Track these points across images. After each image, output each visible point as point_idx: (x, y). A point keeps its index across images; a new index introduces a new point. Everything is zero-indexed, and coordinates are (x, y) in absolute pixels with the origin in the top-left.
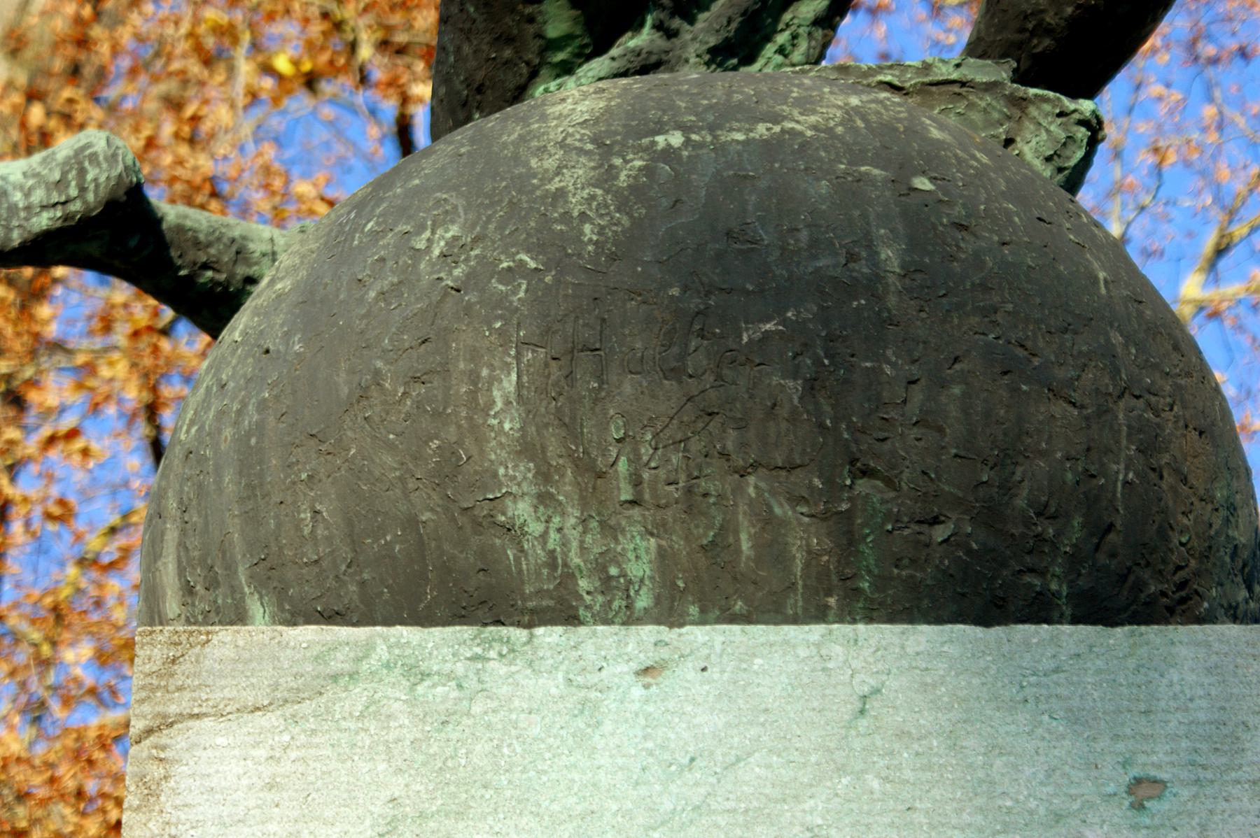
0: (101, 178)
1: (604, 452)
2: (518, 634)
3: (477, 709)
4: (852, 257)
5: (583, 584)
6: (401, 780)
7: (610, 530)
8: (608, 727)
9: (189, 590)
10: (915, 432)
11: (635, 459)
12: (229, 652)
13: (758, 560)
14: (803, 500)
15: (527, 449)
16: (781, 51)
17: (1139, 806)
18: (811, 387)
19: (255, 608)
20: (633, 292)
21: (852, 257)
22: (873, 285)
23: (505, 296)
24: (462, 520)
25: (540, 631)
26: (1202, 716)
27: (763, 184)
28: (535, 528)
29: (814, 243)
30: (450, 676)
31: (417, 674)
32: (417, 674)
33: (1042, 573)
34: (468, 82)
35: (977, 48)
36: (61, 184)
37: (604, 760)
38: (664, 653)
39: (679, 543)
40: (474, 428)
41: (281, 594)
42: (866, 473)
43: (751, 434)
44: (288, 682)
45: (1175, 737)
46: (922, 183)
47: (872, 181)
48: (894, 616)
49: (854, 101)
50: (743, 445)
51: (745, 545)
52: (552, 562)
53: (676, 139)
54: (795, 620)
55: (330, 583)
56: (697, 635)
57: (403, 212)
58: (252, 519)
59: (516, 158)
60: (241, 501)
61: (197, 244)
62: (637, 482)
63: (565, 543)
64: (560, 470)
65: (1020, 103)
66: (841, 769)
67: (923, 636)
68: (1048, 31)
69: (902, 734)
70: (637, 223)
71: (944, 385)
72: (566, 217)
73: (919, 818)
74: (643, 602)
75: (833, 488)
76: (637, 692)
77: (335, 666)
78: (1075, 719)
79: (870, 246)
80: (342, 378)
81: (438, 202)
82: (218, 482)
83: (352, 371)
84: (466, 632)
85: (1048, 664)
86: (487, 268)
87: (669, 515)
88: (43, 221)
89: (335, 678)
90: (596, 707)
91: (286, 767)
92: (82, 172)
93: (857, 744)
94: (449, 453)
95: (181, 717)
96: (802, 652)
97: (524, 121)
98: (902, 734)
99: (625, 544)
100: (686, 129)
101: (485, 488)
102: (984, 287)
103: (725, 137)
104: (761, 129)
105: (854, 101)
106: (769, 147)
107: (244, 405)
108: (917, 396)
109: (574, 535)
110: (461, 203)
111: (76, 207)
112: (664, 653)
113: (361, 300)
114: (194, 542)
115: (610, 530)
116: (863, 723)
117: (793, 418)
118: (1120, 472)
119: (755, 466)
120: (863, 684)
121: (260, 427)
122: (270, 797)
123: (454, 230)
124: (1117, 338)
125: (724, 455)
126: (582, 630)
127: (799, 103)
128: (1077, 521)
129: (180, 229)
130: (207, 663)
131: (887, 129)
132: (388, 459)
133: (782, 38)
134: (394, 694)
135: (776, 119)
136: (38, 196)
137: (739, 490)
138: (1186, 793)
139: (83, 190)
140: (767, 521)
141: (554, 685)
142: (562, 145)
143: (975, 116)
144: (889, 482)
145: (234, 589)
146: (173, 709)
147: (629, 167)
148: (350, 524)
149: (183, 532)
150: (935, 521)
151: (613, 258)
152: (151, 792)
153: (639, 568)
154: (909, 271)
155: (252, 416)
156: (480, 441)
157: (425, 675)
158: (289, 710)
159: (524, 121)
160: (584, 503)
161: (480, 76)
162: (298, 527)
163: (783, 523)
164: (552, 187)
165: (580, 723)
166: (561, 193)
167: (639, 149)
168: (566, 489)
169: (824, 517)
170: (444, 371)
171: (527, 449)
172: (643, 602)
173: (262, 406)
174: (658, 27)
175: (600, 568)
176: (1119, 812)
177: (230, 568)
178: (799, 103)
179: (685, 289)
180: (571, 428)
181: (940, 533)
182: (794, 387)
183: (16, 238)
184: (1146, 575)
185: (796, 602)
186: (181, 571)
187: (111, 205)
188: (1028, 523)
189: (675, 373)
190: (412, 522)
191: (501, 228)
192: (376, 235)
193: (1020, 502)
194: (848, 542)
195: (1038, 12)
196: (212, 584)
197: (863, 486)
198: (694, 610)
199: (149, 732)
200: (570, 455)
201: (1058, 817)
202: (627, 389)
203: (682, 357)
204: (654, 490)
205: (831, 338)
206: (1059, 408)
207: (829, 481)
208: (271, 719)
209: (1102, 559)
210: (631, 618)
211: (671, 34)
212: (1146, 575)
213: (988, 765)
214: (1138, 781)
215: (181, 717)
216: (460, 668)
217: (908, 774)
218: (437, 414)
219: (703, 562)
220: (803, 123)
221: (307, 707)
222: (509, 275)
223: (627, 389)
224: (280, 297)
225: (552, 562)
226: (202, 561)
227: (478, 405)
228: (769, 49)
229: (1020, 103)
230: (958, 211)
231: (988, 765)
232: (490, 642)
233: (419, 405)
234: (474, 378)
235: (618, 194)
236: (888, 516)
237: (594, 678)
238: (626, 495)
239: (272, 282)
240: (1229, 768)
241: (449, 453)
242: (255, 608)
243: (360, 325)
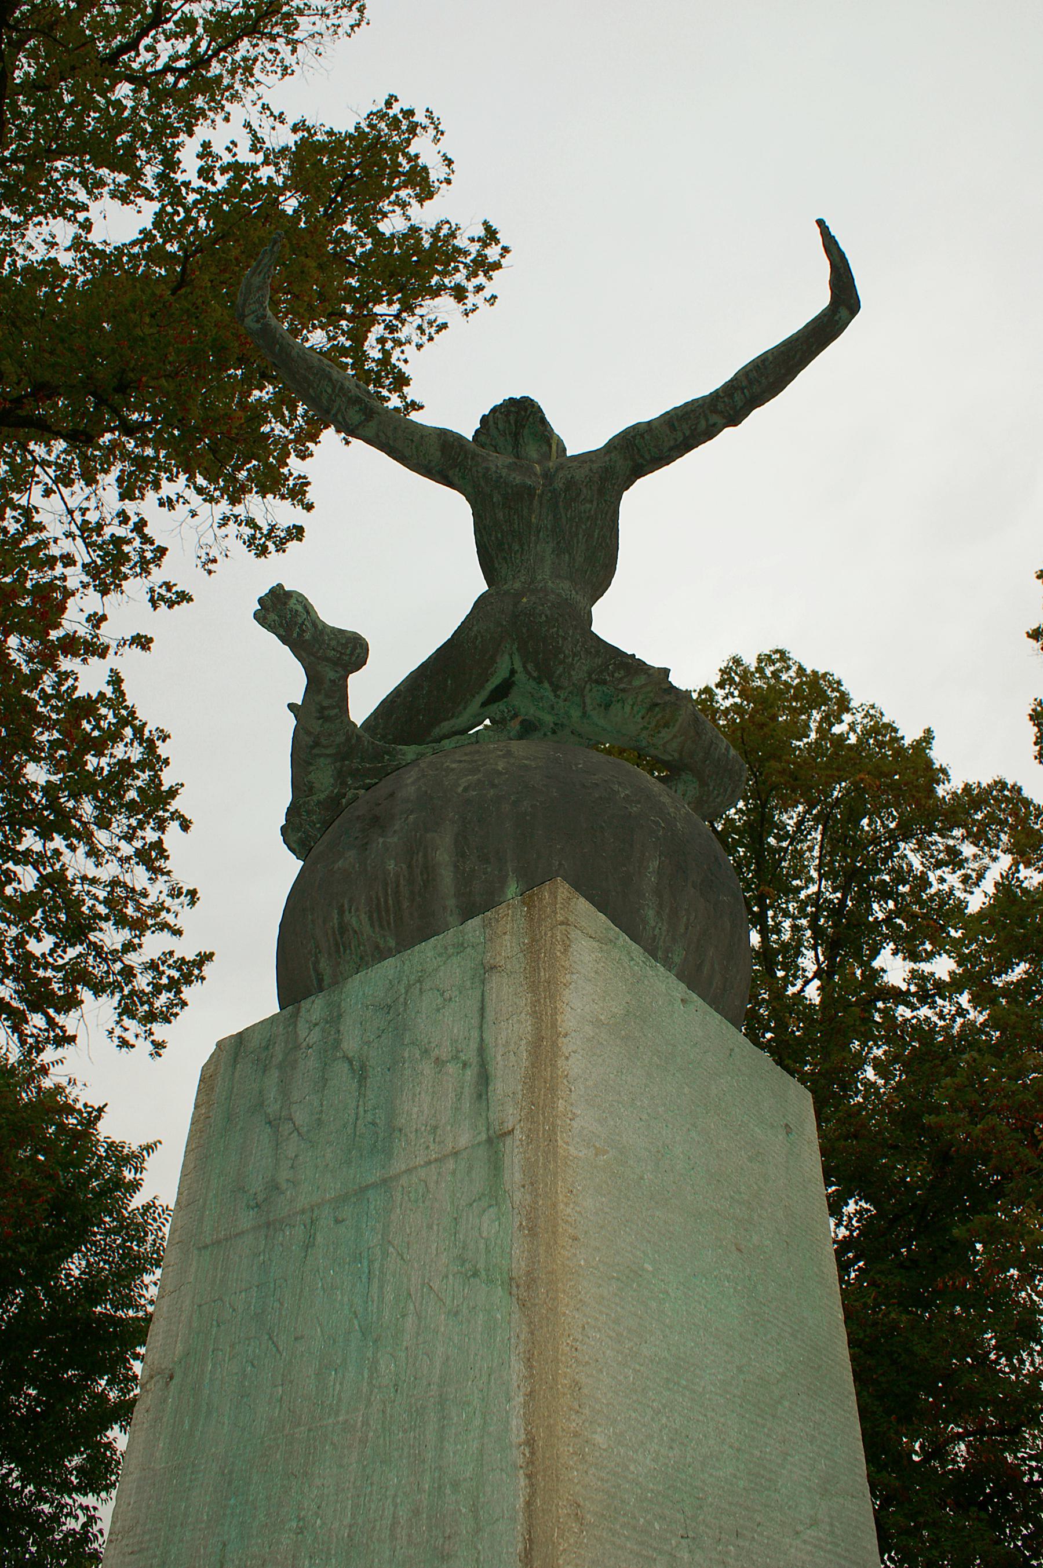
28: (652, 923)
136: (334, 643)
139: (352, 654)
208: (595, 944)
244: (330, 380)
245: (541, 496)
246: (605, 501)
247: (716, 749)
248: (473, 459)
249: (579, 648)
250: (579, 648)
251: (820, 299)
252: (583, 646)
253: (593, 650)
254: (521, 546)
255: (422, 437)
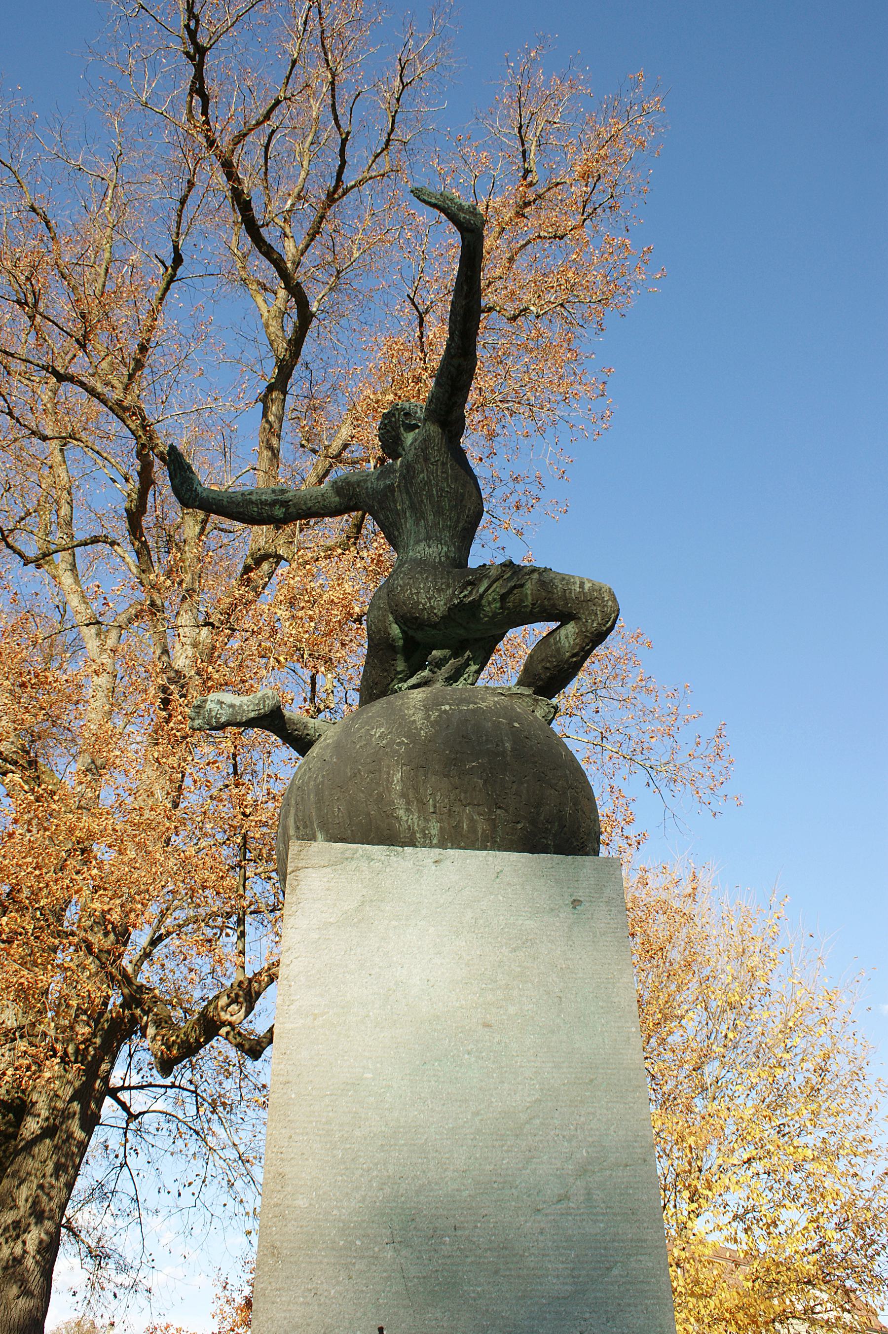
0: (270, 703)
1: (426, 798)
2: (400, 849)
3: (387, 870)
4: (497, 745)
5: (418, 835)
6: (366, 890)
7: (427, 820)
8: (425, 877)
9: (298, 828)
10: (513, 797)
11: (434, 800)
12: (316, 849)
13: (468, 831)
14: (482, 815)
15: (403, 795)
16: (465, 679)
17: (574, 908)
18: (485, 782)
19: (319, 836)
20: (435, 751)
21: (497, 745)
22: (503, 754)
23: (398, 750)
24: (383, 814)
25: (406, 848)
26: (592, 883)
27: (472, 722)
28: (405, 818)
29: (487, 740)
30: (380, 860)
31: (370, 859)
32: (370, 859)
33: (546, 839)
34: (373, 682)
35: (520, 683)
36: (258, 704)
37: (424, 887)
38: (441, 857)
39: (446, 825)
40: (388, 788)
41: (327, 832)
42: (500, 808)
43: (468, 795)
44: (333, 859)
45: (585, 888)
46: (516, 725)
47: (503, 723)
48: (504, 849)
49: (496, 699)
50: (466, 798)
51: (465, 827)
52: (409, 829)
53: (447, 708)
54: (478, 850)
55: (343, 830)
56: (451, 852)
57: (367, 723)
58: (319, 809)
59: (400, 709)
60: (316, 803)
61: (294, 723)
62: (435, 807)
63: (413, 823)
64: (413, 802)
65: (537, 701)
66: (491, 893)
67: (515, 856)
68: (542, 680)
69: (508, 884)
70: (437, 731)
71: (522, 784)
72: (416, 728)
73: (513, 908)
74: (435, 841)
75: (491, 812)
76: (434, 868)
77: (347, 855)
78: (557, 881)
79: (502, 742)
80: (348, 770)
81: (378, 721)
82: (309, 797)
83: (351, 768)
84: (385, 847)
85: (550, 866)
86: (393, 741)
87: (444, 817)
88: (252, 715)
89: (347, 859)
90: (421, 872)
91: (332, 884)
92: (264, 701)
93: (496, 886)
94: (380, 795)
95: (302, 868)
96: (481, 859)
97: (403, 699)
98: (508, 884)
99: (430, 824)
100: (450, 705)
101: (390, 806)
102: (533, 755)
103: (461, 708)
104: (471, 706)
105: (496, 699)
106: (474, 711)
107: (318, 775)
108: (515, 787)
109: (416, 821)
110: (385, 722)
111: (262, 711)
112: (441, 857)
113: (355, 748)
114: (300, 814)
115: (427, 820)
116: (498, 880)
117: (480, 791)
118: (569, 811)
119: (469, 804)
120: (499, 868)
121: (323, 782)
122: (328, 892)
123: (383, 730)
124: (568, 772)
125: (460, 800)
126: (418, 849)
127: (481, 699)
128: (556, 824)
129: (290, 719)
130: (310, 852)
131: (505, 708)
132: (362, 795)
133: (465, 676)
134: (364, 865)
135: (476, 703)
136: (251, 707)
137: (464, 811)
138: (588, 904)
139: (264, 706)
140: (472, 820)
141: (410, 864)
142: (414, 707)
143: (524, 704)
144: (506, 810)
145: (312, 829)
146: (300, 865)
147: (434, 715)
148: (349, 813)
149: (297, 811)
150: (518, 822)
151: (430, 741)
152: (294, 889)
153: (434, 832)
154: (514, 750)
155: (320, 779)
156: (389, 792)
157: (373, 860)
158: (334, 867)
159: (403, 699)
160: (419, 812)
161: (376, 680)
162: (333, 812)
163: (476, 821)
164: (412, 719)
165: (417, 876)
166: (414, 721)
167: (437, 710)
168: (414, 808)
169: (488, 820)
170: (380, 771)
171: (403, 795)
172: (435, 841)
173: (323, 776)
174: (430, 670)
175: (423, 831)
176: (569, 909)
177: (312, 823)
178: (481, 699)
179: (450, 751)
180: (416, 790)
181: (519, 826)
182: (481, 782)
183: (244, 719)
184: (574, 840)
185: (478, 844)
186: (295, 823)
187: (272, 711)
188: (544, 824)
189: (447, 776)
190: (369, 814)
191: (397, 730)
192: (359, 729)
193: (542, 818)
194: (494, 827)
195: (539, 674)
196: (305, 827)
197: (499, 811)
198: (449, 845)
199: (293, 871)
200: (416, 797)
201: (552, 910)
202: (433, 780)
203: (449, 771)
204: (440, 810)
205: (491, 768)
206: (552, 791)
207: (489, 810)
208: (328, 870)
209: (562, 835)
210: (431, 846)
211: (434, 673)
212: (574, 840)
213: (533, 894)
214: (574, 900)
215: (302, 868)
216: (383, 858)
217: (510, 896)
218: (377, 783)
219: (453, 831)
220: (483, 705)
221: (339, 867)
222: (399, 744)
223: (433, 780)
224: (328, 744)
225: (409, 829)
226: (303, 820)
227: (389, 782)
228: (462, 679)
229: (537, 701)
230: (526, 733)
231: (533, 894)
232: (391, 851)
233: (371, 780)
234: (388, 773)
235: (431, 722)
236: (505, 820)
237: (421, 863)
238: (432, 810)
239: (325, 740)
240: (600, 898)
241: (380, 795)
242: (319, 836)
243: (354, 755)
244: (252, 502)
245: (398, 486)
246: (432, 464)
247: (571, 593)
248: (358, 486)
249: (431, 593)
250: (431, 593)
251: (454, 238)
252: (435, 588)
253: (443, 586)
254: (398, 530)
255: (323, 495)
